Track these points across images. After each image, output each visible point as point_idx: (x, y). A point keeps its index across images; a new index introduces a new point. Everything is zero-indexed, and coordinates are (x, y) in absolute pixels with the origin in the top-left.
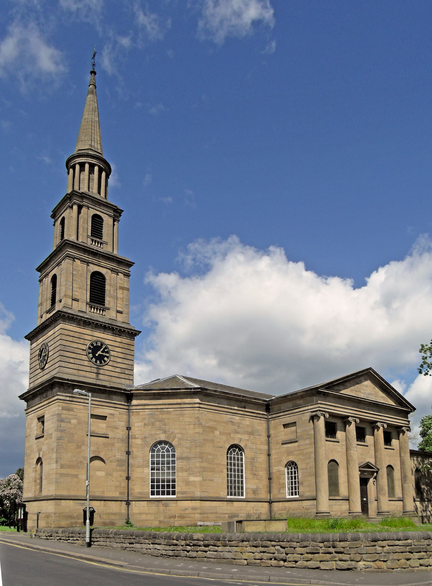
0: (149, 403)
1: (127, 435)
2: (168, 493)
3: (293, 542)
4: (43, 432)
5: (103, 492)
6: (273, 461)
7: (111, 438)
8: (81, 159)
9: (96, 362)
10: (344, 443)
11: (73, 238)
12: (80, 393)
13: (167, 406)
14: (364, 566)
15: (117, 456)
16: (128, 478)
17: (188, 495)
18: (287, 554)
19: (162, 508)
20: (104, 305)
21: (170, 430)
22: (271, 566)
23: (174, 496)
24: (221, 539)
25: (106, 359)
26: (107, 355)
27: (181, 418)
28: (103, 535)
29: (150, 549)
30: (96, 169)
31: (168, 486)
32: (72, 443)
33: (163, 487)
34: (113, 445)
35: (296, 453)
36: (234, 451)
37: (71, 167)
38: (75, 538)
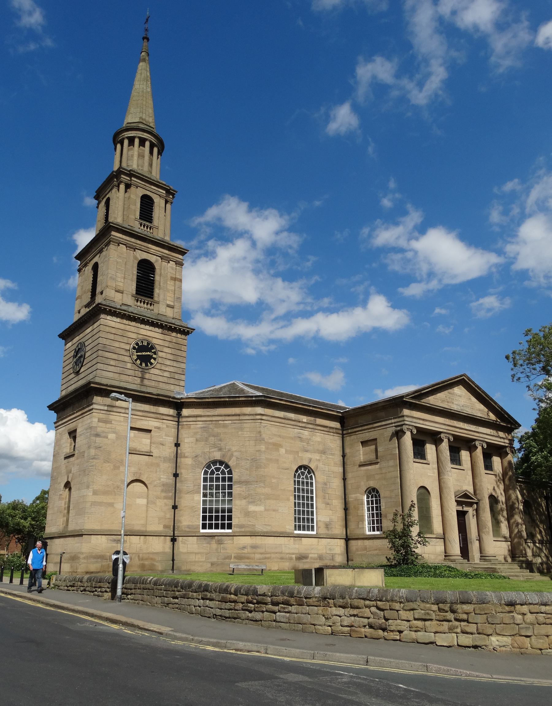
0: (203, 414)
1: (175, 453)
2: (223, 527)
3: (396, 601)
4: (74, 450)
5: (145, 525)
6: (349, 487)
7: (156, 457)
8: (130, 132)
9: (141, 364)
10: (436, 466)
11: (119, 220)
12: (118, 398)
13: (223, 418)
14: (497, 643)
15: (162, 480)
16: (175, 507)
17: (247, 529)
18: (387, 620)
19: (214, 545)
20: (152, 298)
21: (227, 447)
22: (366, 637)
23: (230, 531)
24: (295, 595)
25: (152, 361)
26: (154, 356)
27: (240, 433)
28: (138, 585)
29: (200, 607)
30: (147, 144)
31: (223, 518)
32: (109, 462)
33: (217, 518)
34: (158, 465)
35: (377, 477)
36: (303, 473)
37: (118, 142)
38: (104, 590)
